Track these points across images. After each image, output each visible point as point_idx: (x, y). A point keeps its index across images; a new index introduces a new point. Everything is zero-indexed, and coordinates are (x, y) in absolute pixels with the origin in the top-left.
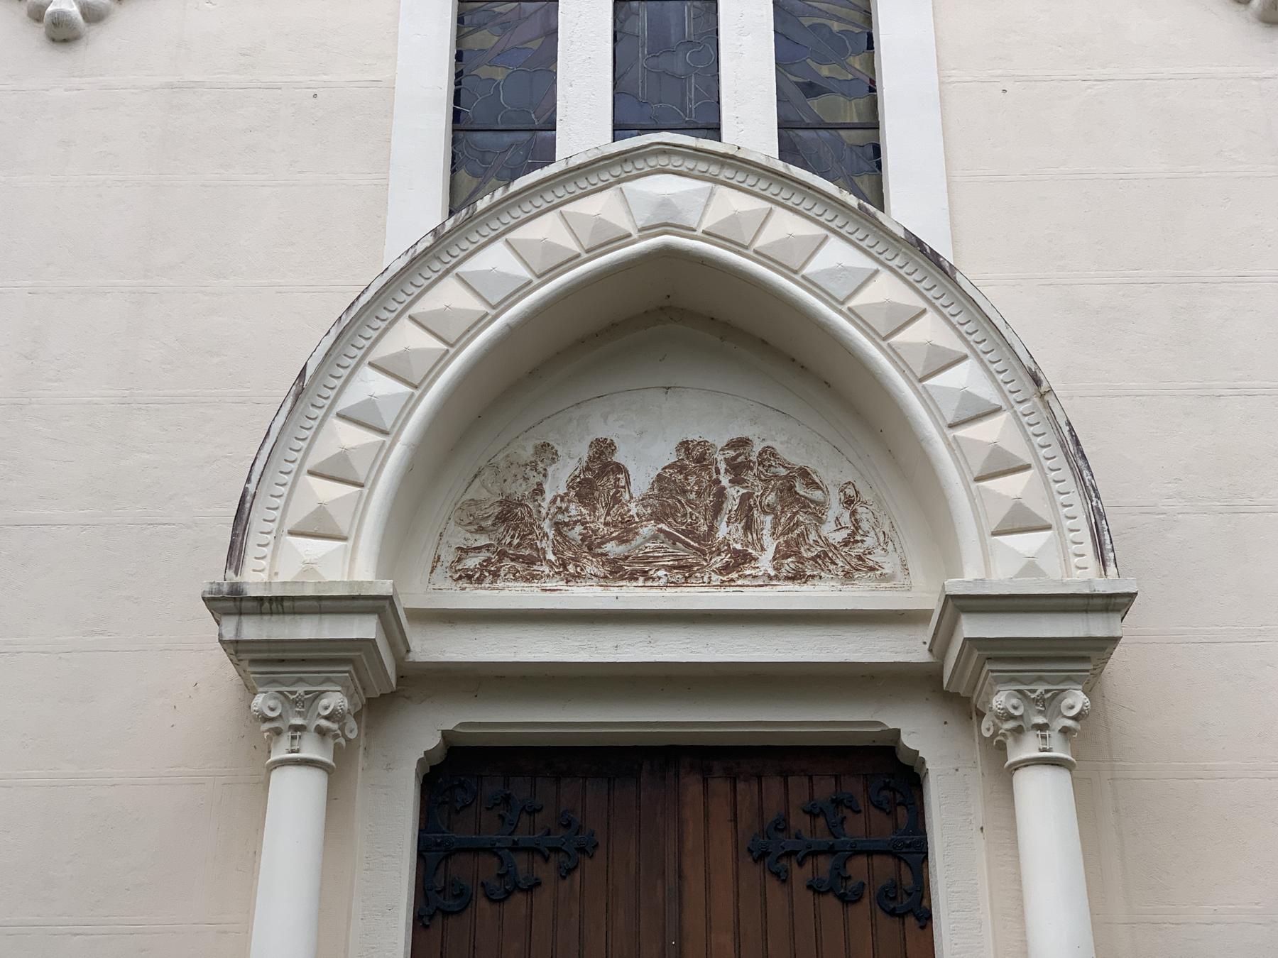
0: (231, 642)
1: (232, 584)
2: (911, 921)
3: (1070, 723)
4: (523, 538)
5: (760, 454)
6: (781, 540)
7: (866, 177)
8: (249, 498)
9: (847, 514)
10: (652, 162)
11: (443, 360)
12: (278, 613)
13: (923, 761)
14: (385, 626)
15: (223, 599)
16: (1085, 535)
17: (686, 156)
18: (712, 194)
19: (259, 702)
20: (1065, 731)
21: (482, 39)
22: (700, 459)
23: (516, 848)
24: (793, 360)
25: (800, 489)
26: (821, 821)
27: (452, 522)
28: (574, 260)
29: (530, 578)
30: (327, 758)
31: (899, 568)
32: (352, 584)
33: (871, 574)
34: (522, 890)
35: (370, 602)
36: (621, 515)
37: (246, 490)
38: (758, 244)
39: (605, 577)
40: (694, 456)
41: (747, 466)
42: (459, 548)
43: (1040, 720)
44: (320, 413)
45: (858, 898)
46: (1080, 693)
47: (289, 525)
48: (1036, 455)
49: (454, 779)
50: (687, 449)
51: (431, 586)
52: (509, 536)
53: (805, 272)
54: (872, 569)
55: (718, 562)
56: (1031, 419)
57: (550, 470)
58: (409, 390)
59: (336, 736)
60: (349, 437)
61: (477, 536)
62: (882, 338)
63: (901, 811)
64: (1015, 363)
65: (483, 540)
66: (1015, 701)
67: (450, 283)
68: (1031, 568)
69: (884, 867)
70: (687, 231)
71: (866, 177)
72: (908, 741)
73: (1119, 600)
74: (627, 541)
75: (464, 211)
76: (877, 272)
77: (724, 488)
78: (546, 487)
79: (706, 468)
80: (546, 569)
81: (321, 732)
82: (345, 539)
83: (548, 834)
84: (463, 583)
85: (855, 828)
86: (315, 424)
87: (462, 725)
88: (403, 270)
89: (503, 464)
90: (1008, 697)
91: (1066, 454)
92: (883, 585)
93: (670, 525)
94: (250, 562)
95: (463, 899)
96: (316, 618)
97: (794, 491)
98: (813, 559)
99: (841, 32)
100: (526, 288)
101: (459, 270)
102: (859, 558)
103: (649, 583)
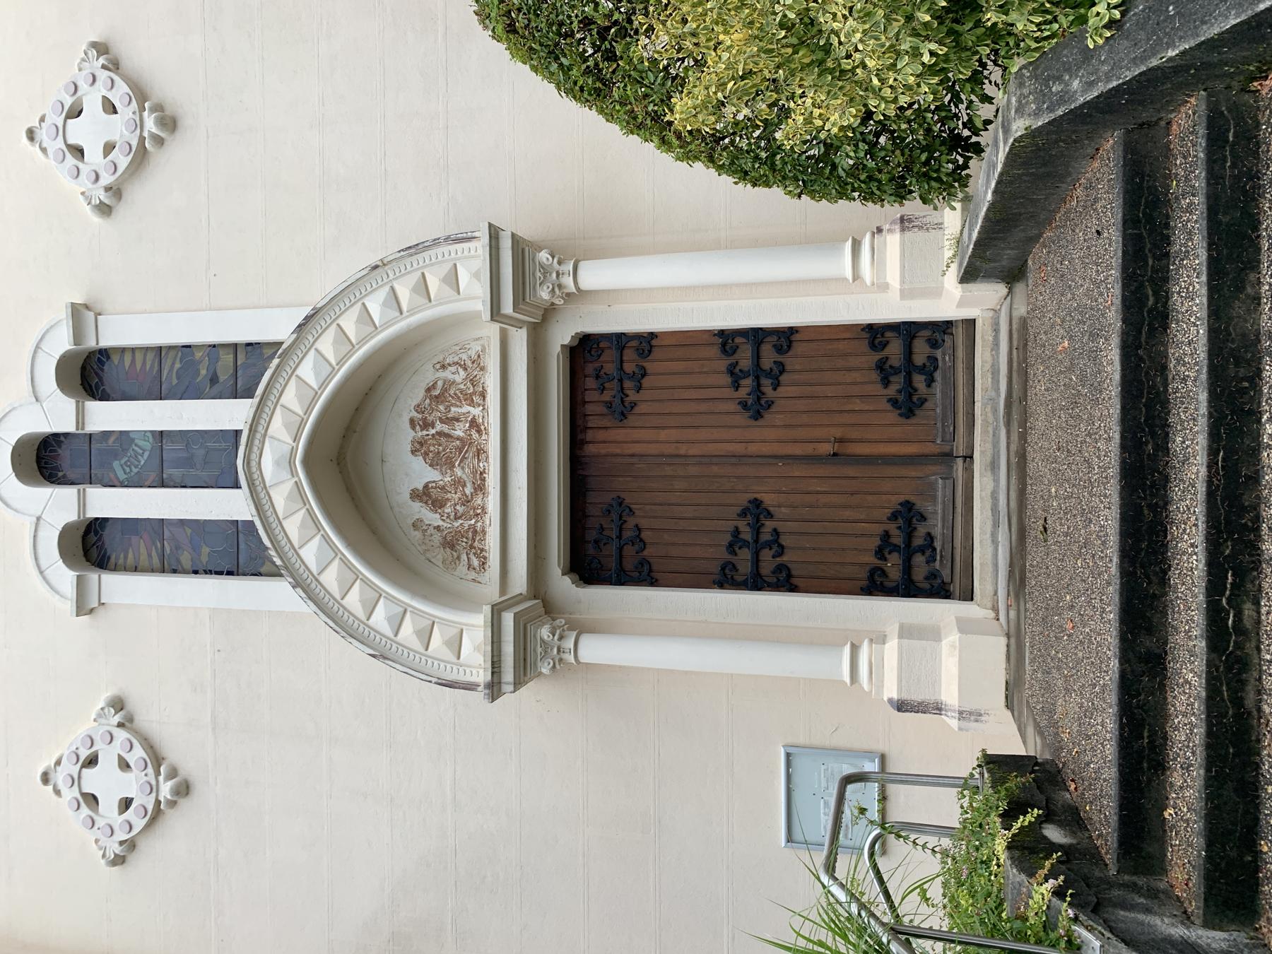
2: (654, 342)
10: (254, 469)
11: (365, 581)
16: (459, 246)
18: (272, 437)
20: (560, 263)
21: (186, 559)
22: (421, 444)
23: (620, 537)
25: (437, 392)
28: (310, 512)
29: (484, 532)
32: (485, 626)
40: (419, 447)
41: (424, 420)
43: (554, 275)
44: (394, 646)
45: (643, 368)
49: (588, 565)
52: (460, 544)
53: (316, 387)
55: (475, 435)
56: (397, 271)
58: (382, 600)
60: (407, 630)
62: (353, 348)
63: (602, 345)
65: (464, 557)
68: (476, 275)
69: (629, 354)
70: (293, 452)
72: (567, 341)
81: (561, 638)
85: (610, 368)
88: (315, 603)
94: (474, 679)
95: (644, 562)
97: (438, 396)
99: (181, 361)
101: (315, 573)
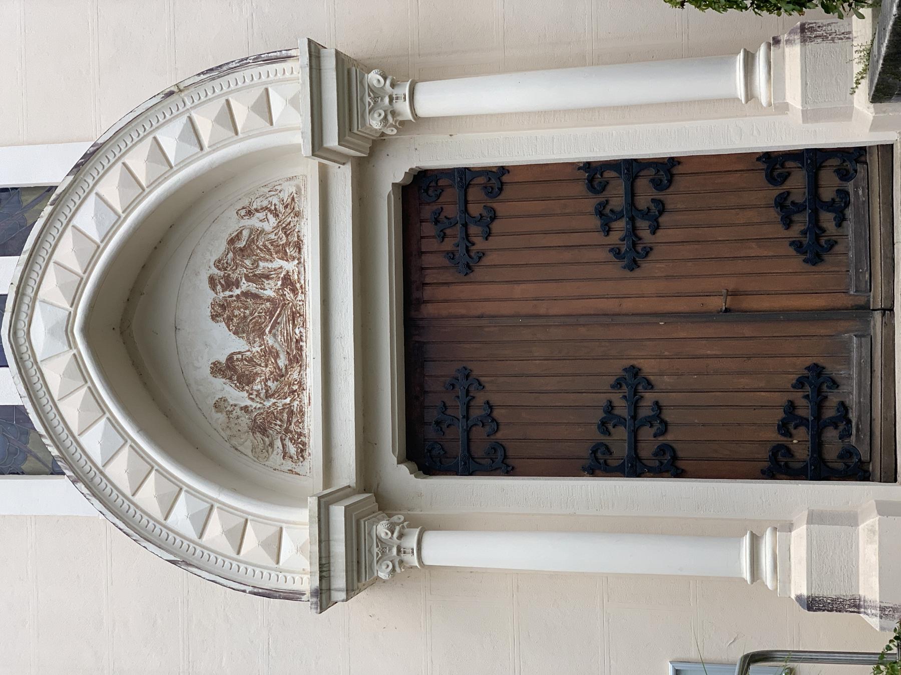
0: (347, 594)
1: (312, 596)
2: (505, 178)
3: (388, 82)
4: (276, 418)
5: (219, 269)
6: (275, 256)
7: (23, 198)
8: (256, 590)
9: (257, 215)
12: (329, 566)
13: (411, 169)
14: (336, 501)
15: (321, 601)
16: (272, 67)
17: (17, 319)
18: (44, 301)
19: (383, 574)
20: (393, 85)
22: (223, 307)
23: (467, 417)
24: (156, 248)
25: (242, 244)
26: (448, 231)
27: (267, 463)
28: (93, 391)
29: (302, 412)
30: (417, 532)
31: (292, 182)
33: (296, 200)
34: (491, 412)
35: (322, 510)
36: (260, 357)
37: (250, 593)
38: (80, 271)
39: (301, 366)
40: (220, 312)
42: (284, 458)
43: (387, 100)
44: (199, 550)
46: (370, 75)
47: (272, 564)
48: (219, 96)
50: (217, 316)
51: (308, 474)
52: (274, 427)
54: (293, 199)
55: (289, 295)
56: (196, 98)
57: (232, 402)
58: (183, 494)
59: (403, 527)
60: (215, 531)
61: (276, 447)
62: (143, 191)
63: (441, 183)
64: (159, 107)
65: (278, 443)
66: (376, 115)
67: (109, 471)
68: (293, 102)
69: (475, 194)
70: (71, 318)
71: (23, 198)
73: (313, 50)
74: (277, 353)
75: (59, 463)
76: (97, 194)
77: (242, 292)
78: (243, 405)
79: (229, 304)
80: (296, 403)
81: (401, 536)
82: (281, 529)
83: (458, 397)
84: (306, 454)
85: (452, 211)
86: (206, 552)
87: (394, 452)
88: (101, 501)
89: (228, 432)
90: (373, 119)
91: (219, 77)
92: (303, 192)
93: (267, 326)
95: (497, 447)
96: (332, 543)
97: (243, 248)
98: (287, 236)
100: (113, 422)
101: (100, 465)
102: (286, 207)
103: (304, 339)
